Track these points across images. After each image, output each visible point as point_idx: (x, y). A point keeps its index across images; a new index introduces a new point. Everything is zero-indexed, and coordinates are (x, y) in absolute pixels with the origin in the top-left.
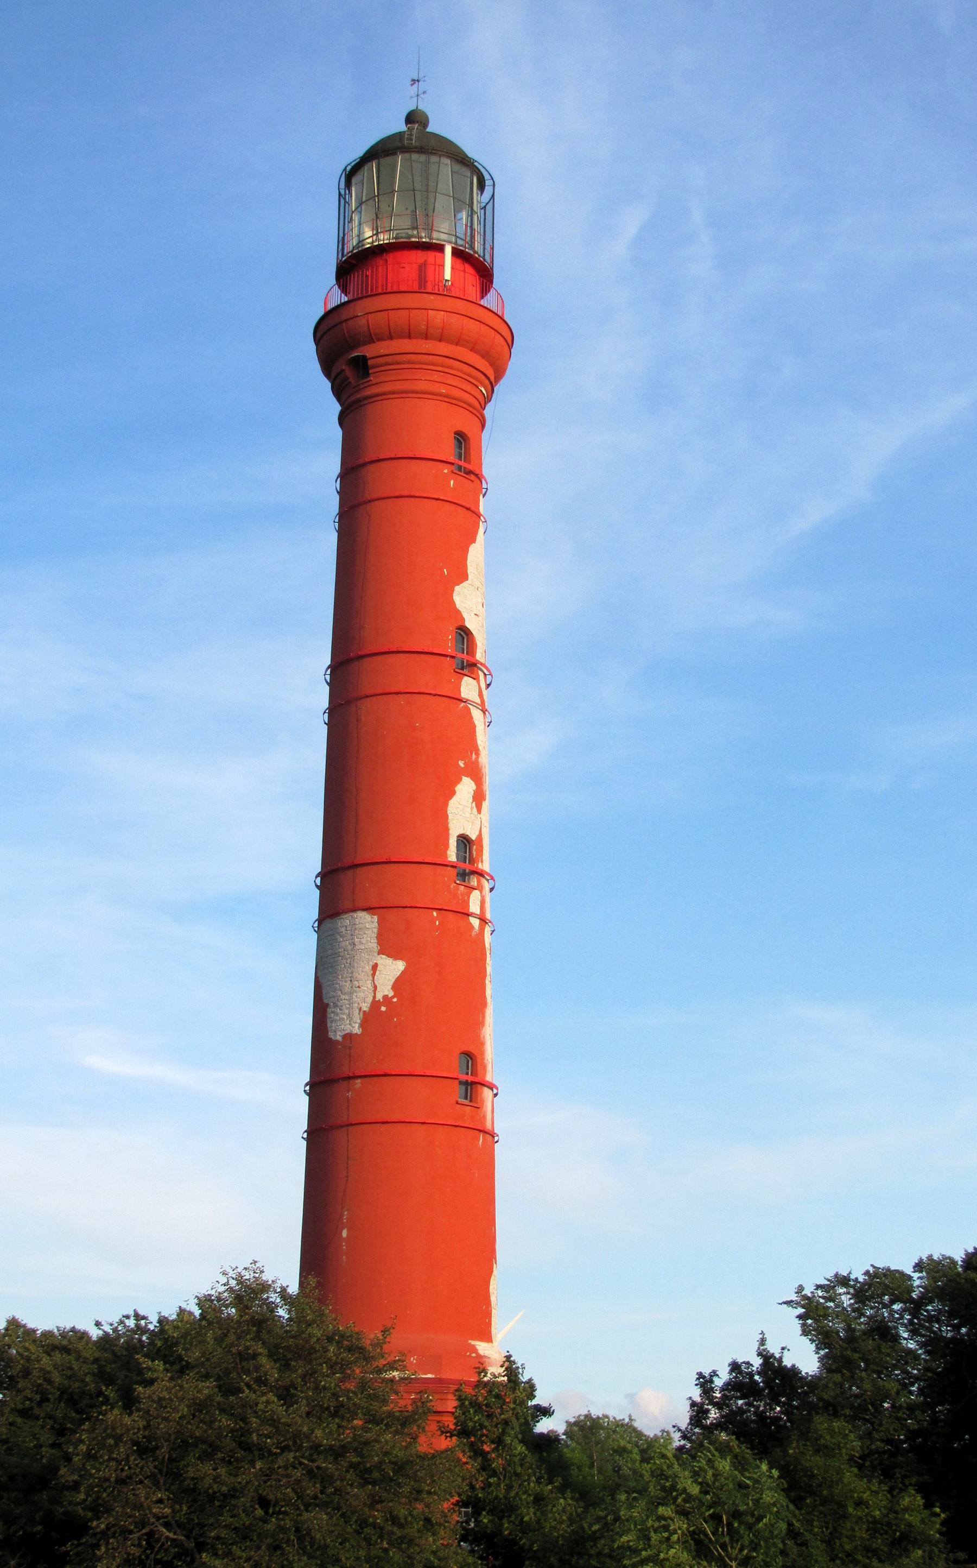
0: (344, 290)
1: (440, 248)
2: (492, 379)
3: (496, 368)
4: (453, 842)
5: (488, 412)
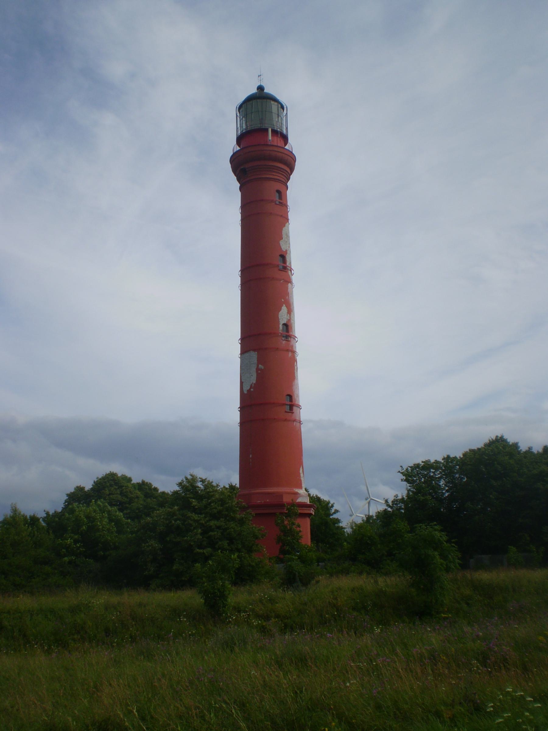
0: (240, 147)
1: (267, 130)
2: (289, 172)
3: (292, 169)
4: (281, 327)
5: (289, 184)
